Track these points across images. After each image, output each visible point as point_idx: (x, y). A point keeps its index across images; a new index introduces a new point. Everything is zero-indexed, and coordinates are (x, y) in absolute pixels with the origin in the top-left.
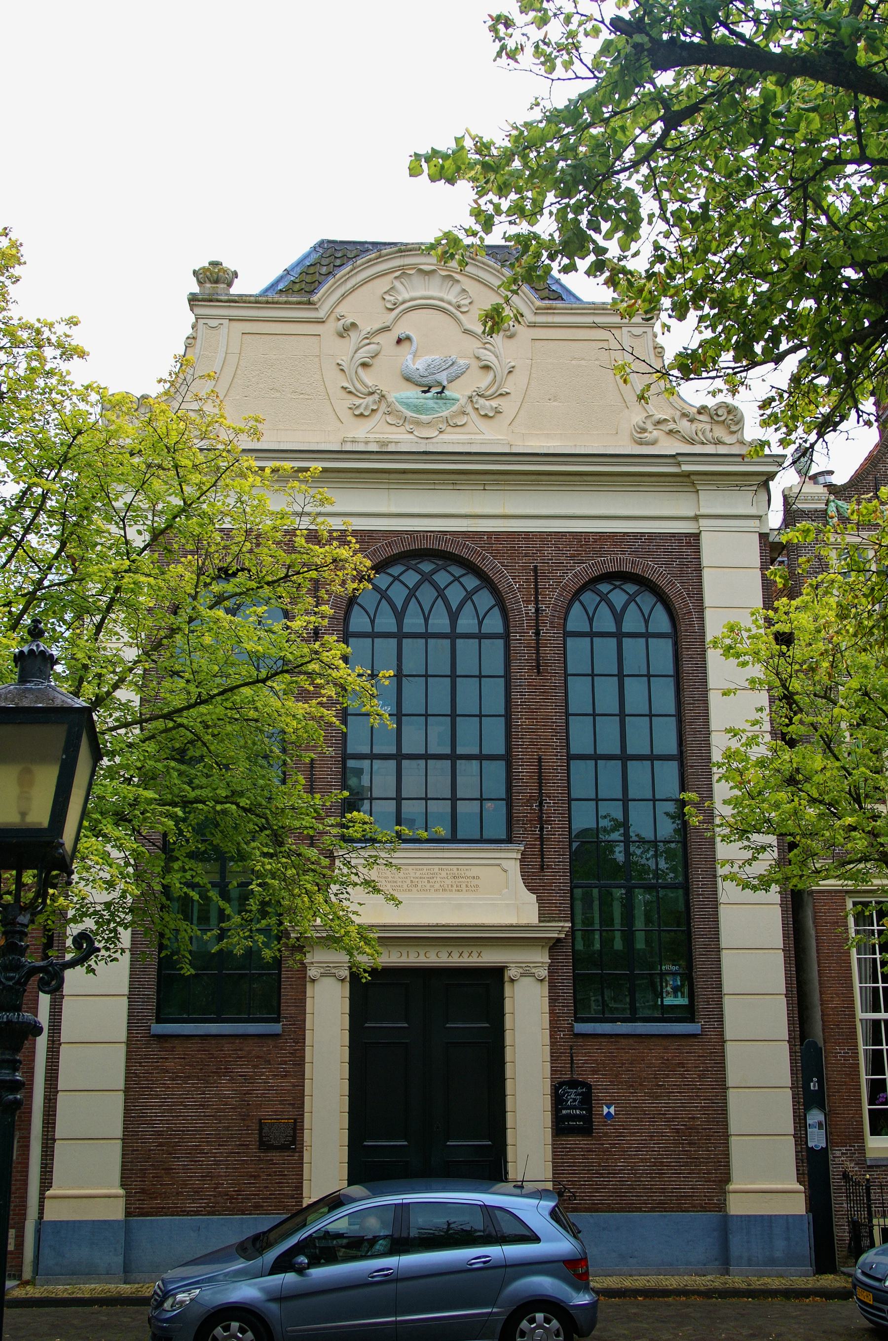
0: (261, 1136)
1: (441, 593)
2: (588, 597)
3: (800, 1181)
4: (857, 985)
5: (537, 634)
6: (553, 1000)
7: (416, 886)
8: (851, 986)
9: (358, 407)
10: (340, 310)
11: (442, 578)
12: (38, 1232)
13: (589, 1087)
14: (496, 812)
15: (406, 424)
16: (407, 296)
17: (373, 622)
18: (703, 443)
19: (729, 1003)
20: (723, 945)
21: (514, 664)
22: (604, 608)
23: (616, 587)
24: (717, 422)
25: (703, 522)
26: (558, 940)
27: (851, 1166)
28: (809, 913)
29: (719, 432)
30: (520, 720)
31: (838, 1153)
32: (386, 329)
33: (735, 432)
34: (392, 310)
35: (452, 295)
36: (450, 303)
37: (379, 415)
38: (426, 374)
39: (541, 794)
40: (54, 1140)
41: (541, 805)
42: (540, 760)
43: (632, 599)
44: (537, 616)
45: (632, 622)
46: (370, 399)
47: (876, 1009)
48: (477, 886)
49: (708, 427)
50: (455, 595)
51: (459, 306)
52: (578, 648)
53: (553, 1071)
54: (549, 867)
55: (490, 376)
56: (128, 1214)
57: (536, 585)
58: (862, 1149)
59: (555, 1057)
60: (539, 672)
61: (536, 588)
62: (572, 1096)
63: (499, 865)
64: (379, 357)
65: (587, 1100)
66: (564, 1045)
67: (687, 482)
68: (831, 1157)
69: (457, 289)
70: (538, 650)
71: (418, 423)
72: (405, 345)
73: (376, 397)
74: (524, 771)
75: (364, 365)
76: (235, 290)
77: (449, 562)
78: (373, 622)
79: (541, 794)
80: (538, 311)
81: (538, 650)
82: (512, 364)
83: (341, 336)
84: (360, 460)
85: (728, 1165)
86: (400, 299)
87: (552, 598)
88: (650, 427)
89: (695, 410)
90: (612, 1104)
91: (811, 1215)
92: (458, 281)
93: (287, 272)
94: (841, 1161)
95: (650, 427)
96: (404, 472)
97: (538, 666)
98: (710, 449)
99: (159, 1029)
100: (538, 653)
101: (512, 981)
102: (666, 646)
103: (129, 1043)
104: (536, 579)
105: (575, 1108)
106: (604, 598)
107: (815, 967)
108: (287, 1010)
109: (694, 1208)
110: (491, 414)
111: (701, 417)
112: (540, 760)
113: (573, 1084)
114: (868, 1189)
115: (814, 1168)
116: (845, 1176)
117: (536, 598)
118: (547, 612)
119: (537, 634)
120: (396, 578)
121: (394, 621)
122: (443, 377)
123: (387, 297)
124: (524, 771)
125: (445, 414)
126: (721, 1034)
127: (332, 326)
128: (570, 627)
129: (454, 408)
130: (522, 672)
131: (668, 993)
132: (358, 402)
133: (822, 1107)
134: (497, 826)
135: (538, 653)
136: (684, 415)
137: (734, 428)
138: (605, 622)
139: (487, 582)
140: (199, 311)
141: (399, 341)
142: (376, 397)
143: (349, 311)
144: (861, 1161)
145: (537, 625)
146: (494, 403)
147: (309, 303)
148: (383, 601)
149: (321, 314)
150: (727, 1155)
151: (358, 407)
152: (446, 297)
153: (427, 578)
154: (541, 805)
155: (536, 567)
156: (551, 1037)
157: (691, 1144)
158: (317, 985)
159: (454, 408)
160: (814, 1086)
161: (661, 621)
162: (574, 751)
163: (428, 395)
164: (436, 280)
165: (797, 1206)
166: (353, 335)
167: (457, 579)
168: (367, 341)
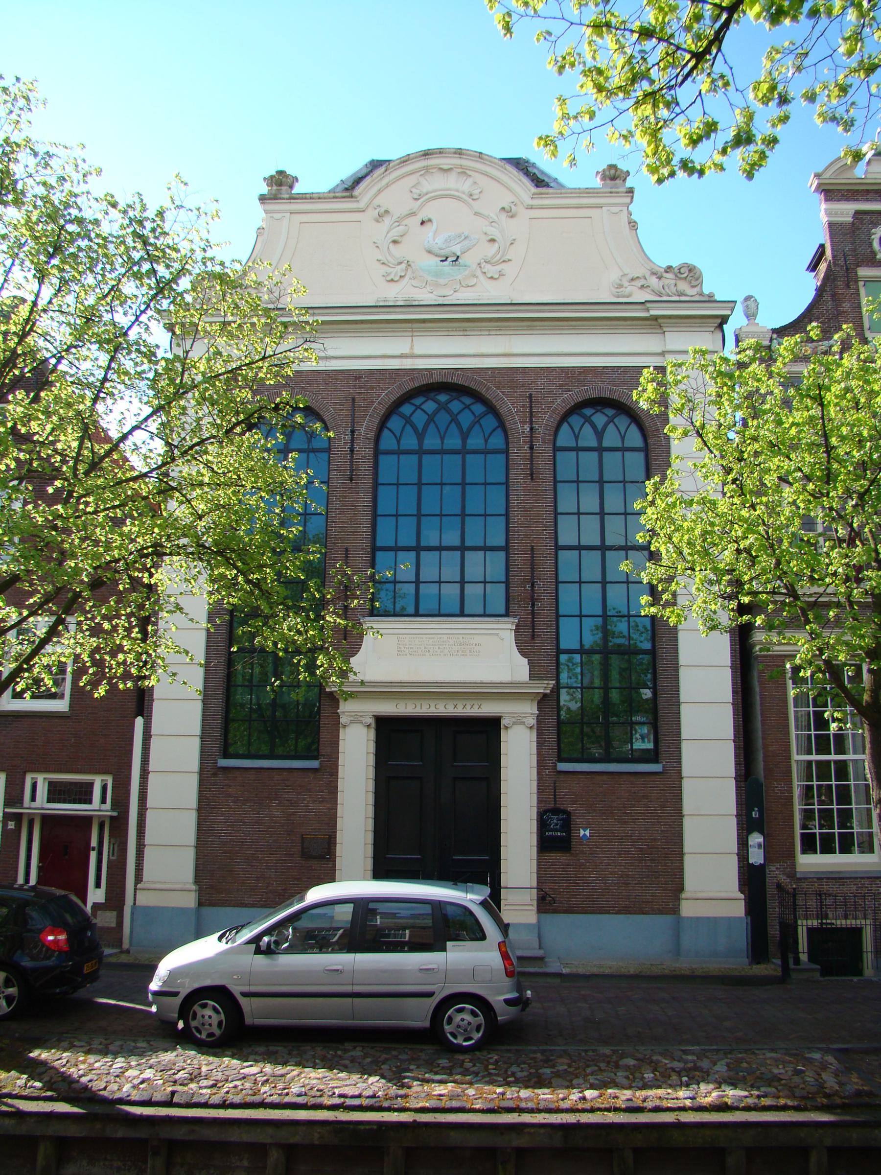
0: (303, 848)
1: (454, 419)
2: (575, 420)
3: (741, 890)
4: (793, 732)
5: (531, 448)
6: (540, 744)
7: (429, 651)
8: (787, 734)
10: (376, 202)
11: (455, 406)
12: (132, 914)
13: (569, 814)
14: (497, 594)
15: (427, 286)
16: (430, 189)
17: (398, 442)
19: (685, 746)
20: (681, 701)
21: (512, 472)
22: (587, 428)
24: (681, 279)
26: (545, 695)
27: (783, 879)
28: (755, 675)
29: (683, 286)
30: (517, 517)
31: (773, 868)
32: (413, 214)
33: (695, 286)
35: (466, 186)
36: (464, 193)
37: (406, 279)
38: (443, 247)
39: (533, 577)
40: (145, 846)
41: (533, 585)
42: (532, 549)
43: (611, 420)
44: (531, 434)
45: (611, 439)
46: (400, 267)
47: (809, 753)
48: (479, 652)
49: (673, 282)
50: (466, 419)
52: (566, 461)
53: (540, 801)
54: (539, 636)
55: (496, 245)
56: (201, 904)
58: (793, 865)
59: (541, 790)
61: (531, 412)
62: (554, 820)
63: (497, 635)
65: (567, 824)
66: (548, 781)
67: (656, 324)
68: (767, 871)
69: (470, 181)
70: (532, 461)
72: (427, 226)
73: (404, 266)
74: (519, 559)
75: (395, 242)
78: (398, 442)
79: (533, 577)
81: (532, 461)
83: (378, 221)
85: (682, 878)
86: (425, 191)
87: (545, 420)
88: (626, 284)
90: (587, 828)
91: (749, 918)
92: (470, 176)
94: (775, 874)
95: (626, 284)
96: (424, 321)
97: (532, 475)
99: (223, 762)
100: (531, 464)
101: (506, 728)
102: (640, 457)
103: (201, 772)
105: (557, 831)
107: (759, 717)
108: (324, 750)
109: (653, 912)
110: (496, 276)
111: (667, 275)
112: (532, 549)
113: (556, 811)
114: (794, 896)
115: (752, 879)
116: (779, 886)
117: (531, 420)
118: (540, 430)
119: (531, 448)
120: (418, 407)
121: (416, 442)
122: (457, 250)
123: (414, 190)
124: (519, 559)
125: (459, 277)
126: (680, 772)
127: (372, 213)
128: (560, 443)
129: (467, 272)
130: (518, 478)
131: (637, 739)
132: (389, 270)
133: (761, 832)
134: (498, 603)
135: (531, 464)
136: (653, 273)
137: (694, 283)
138: (588, 438)
139: (491, 409)
140: (270, 207)
141: (423, 223)
142: (404, 266)
143: (385, 200)
144: (792, 874)
145: (531, 442)
146: (499, 268)
147: (352, 197)
148: (453, 425)
149: (362, 205)
150: (681, 869)
151: (388, 274)
153: (443, 407)
154: (533, 585)
155: (531, 395)
156: (539, 773)
157: (652, 860)
158: (348, 730)
159: (467, 272)
160: (755, 814)
161: (634, 438)
162: (561, 542)
164: (453, 176)
165: (738, 909)
166: (387, 220)
167: (467, 407)
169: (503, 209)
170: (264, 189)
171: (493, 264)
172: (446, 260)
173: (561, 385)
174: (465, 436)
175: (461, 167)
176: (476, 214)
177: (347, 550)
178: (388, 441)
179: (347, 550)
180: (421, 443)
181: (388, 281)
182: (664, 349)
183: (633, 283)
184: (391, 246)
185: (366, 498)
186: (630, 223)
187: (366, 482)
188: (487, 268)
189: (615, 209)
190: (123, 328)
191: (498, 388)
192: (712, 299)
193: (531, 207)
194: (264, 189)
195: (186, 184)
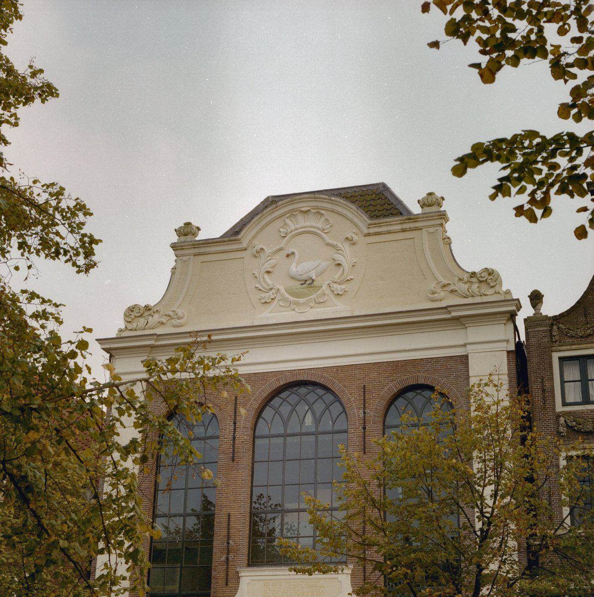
9: (264, 298)
10: (255, 242)
11: (311, 397)
16: (293, 227)
18: (473, 296)
23: (418, 394)
32: (281, 249)
34: (285, 237)
36: (318, 229)
51: (324, 230)
57: (364, 397)
64: (277, 266)
69: (323, 219)
71: (297, 304)
73: (273, 291)
75: (268, 272)
76: (201, 236)
88: (439, 290)
92: (323, 214)
98: (477, 300)
106: (410, 402)
123: (282, 230)
132: (263, 295)
137: (492, 284)
139: (338, 399)
140: (179, 252)
149: (244, 245)
153: (303, 399)
159: (319, 292)
163: (304, 286)
167: (320, 397)
168: (269, 258)
169: (347, 238)
170: (175, 239)
171: (340, 283)
172: (305, 283)
175: (317, 208)
176: (328, 245)
177: (229, 515)
178: (262, 428)
180: (285, 429)
182: (466, 342)
185: (245, 474)
186: (444, 239)
187: (245, 460)
188: (336, 286)
189: (432, 230)
191: (340, 382)
192: (508, 298)
193: (368, 235)
194: (175, 239)
195: (91, 354)
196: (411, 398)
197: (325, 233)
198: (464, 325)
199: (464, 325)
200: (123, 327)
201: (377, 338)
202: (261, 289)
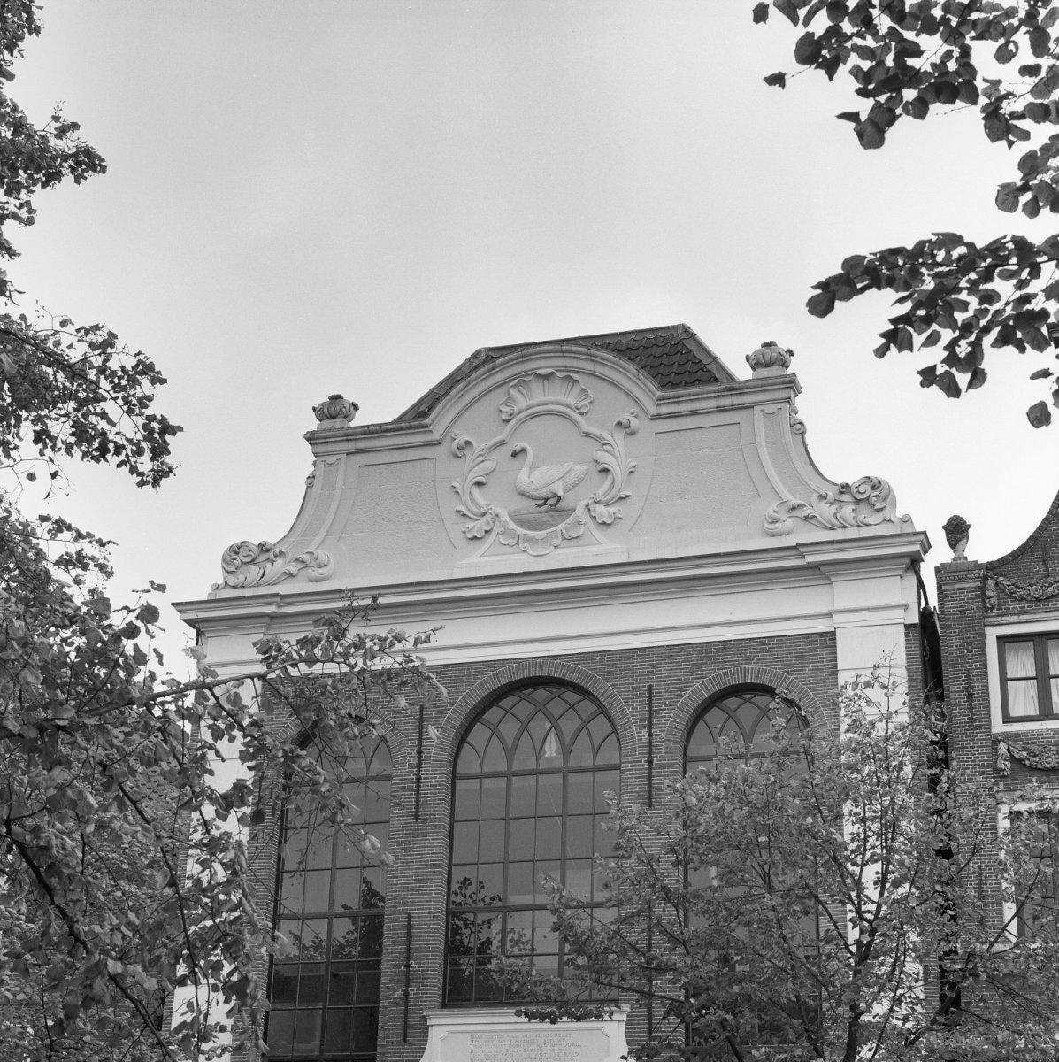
5: (650, 762)
11: (556, 707)
16: (523, 404)
18: (844, 527)
23: (746, 701)
25: (836, 617)
29: (865, 515)
37: (493, 535)
57: (650, 707)
60: (650, 805)
67: (819, 573)
69: (576, 389)
75: (479, 484)
76: (359, 420)
77: (564, 689)
80: (660, 401)
82: (634, 463)
84: (889, 545)
88: (783, 515)
89: (836, 489)
92: (577, 381)
93: (714, 359)
97: (650, 797)
98: (852, 533)
104: (650, 700)
106: (731, 716)
119: (650, 762)
123: (504, 409)
132: (471, 524)
137: (878, 506)
139: (602, 710)
140: (321, 449)
146: (612, 510)
147: (422, 427)
148: (494, 737)
149: (436, 436)
152: (535, 401)
153: (541, 709)
155: (650, 686)
167: (572, 707)
168: (481, 458)
169: (619, 424)
170: (313, 424)
171: (607, 505)
172: (544, 504)
173: (692, 670)
174: (510, 753)
176: (586, 435)
177: (409, 917)
178: (469, 762)
179: (409, 917)
181: (470, 539)
183: (794, 513)
184: (475, 490)
185: (438, 843)
186: (792, 425)
188: (600, 509)
189: (771, 408)
190: (535, 950)
192: (908, 530)
193: (657, 417)
194: (313, 424)
196: (733, 708)
197: (581, 414)
198: (828, 578)
199: (828, 578)
200: (221, 582)
201: (657, 603)
202: (467, 513)
